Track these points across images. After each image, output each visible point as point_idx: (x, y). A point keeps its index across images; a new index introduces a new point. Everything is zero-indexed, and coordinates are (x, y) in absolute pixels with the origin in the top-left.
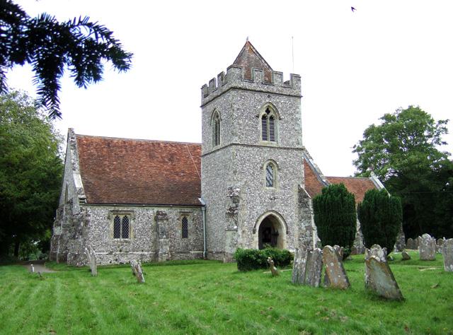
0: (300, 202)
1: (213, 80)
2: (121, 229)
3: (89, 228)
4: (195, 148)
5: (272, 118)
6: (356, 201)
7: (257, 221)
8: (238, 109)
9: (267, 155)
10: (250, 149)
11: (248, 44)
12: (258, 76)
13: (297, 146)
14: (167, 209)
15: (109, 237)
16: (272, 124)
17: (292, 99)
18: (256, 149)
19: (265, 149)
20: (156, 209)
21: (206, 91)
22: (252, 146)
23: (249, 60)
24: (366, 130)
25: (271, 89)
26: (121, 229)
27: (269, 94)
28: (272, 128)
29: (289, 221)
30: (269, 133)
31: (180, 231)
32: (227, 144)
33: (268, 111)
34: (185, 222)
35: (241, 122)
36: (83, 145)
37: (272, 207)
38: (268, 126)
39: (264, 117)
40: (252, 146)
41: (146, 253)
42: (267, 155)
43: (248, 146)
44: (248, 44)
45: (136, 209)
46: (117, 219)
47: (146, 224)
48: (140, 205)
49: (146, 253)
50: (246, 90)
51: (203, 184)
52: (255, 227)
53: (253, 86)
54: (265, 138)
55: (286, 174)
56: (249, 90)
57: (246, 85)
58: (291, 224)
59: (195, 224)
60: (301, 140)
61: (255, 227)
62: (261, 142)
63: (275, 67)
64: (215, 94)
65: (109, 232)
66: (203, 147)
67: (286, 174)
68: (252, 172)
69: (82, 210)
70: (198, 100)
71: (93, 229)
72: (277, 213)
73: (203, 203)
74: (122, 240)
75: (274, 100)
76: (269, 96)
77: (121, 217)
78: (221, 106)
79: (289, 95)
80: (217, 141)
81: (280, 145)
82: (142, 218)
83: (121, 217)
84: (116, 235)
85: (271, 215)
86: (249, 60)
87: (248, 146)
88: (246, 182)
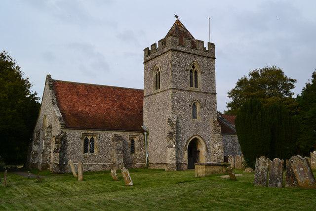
0: (215, 130)
1: (155, 44)
2: (88, 146)
3: (67, 146)
4: (141, 92)
7: (187, 142)
8: (175, 65)
9: (193, 96)
10: (183, 92)
11: (178, 24)
12: (189, 44)
14: (121, 133)
15: (80, 153)
17: (209, 59)
18: (187, 93)
20: (114, 133)
21: (148, 52)
22: (184, 90)
23: (179, 33)
25: (196, 52)
26: (88, 146)
28: (196, 79)
30: (193, 82)
31: (130, 149)
32: (166, 88)
34: (133, 142)
35: (177, 73)
36: (53, 85)
38: (194, 78)
39: (191, 71)
41: (107, 164)
42: (193, 96)
43: (181, 90)
44: (178, 24)
45: (100, 132)
47: (107, 143)
48: (103, 129)
49: (107, 164)
50: (180, 51)
51: (145, 116)
52: (186, 146)
53: (185, 49)
54: (191, 86)
56: (182, 52)
57: (180, 48)
59: (140, 144)
60: (215, 87)
61: (186, 146)
62: (156, 91)
63: (197, 37)
64: (156, 54)
65: (80, 148)
66: (145, 91)
68: (184, 108)
69: (62, 132)
70: (141, 58)
71: (69, 146)
73: (145, 129)
74: (90, 154)
75: (199, 59)
76: (195, 57)
77: (89, 138)
78: (162, 62)
79: (208, 57)
80: (157, 86)
82: (104, 138)
83: (89, 138)
84: (86, 151)
85: (196, 138)
86: (179, 33)
87: (181, 90)
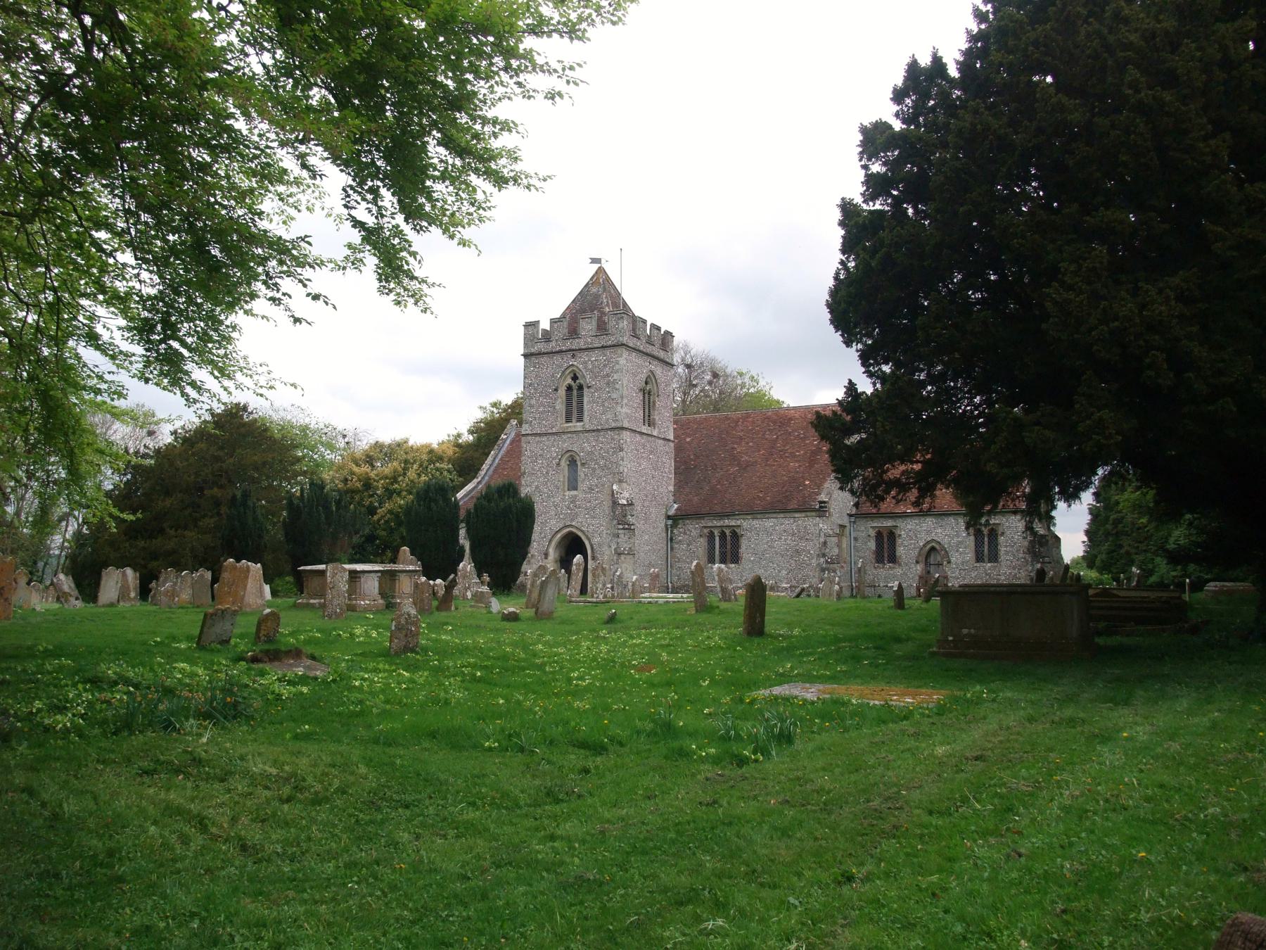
5: (581, 388)
6: (330, 566)
10: (544, 439)
13: (613, 425)
16: (581, 396)
19: (564, 437)
22: (546, 434)
24: (834, 293)
27: (573, 352)
28: (580, 403)
29: (596, 540)
30: (574, 409)
33: (575, 378)
35: (533, 402)
37: (572, 520)
38: (575, 399)
39: (569, 388)
40: (546, 434)
42: (566, 443)
43: (540, 435)
46: (711, 537)
55: (594, 470)
58: (600, 545)
67: (594, 470)
72: (550, 541)
76: (573, 356)
77: (727, 532)
81: (587, 427)
87: (540, 435)
88: (537, 487)
